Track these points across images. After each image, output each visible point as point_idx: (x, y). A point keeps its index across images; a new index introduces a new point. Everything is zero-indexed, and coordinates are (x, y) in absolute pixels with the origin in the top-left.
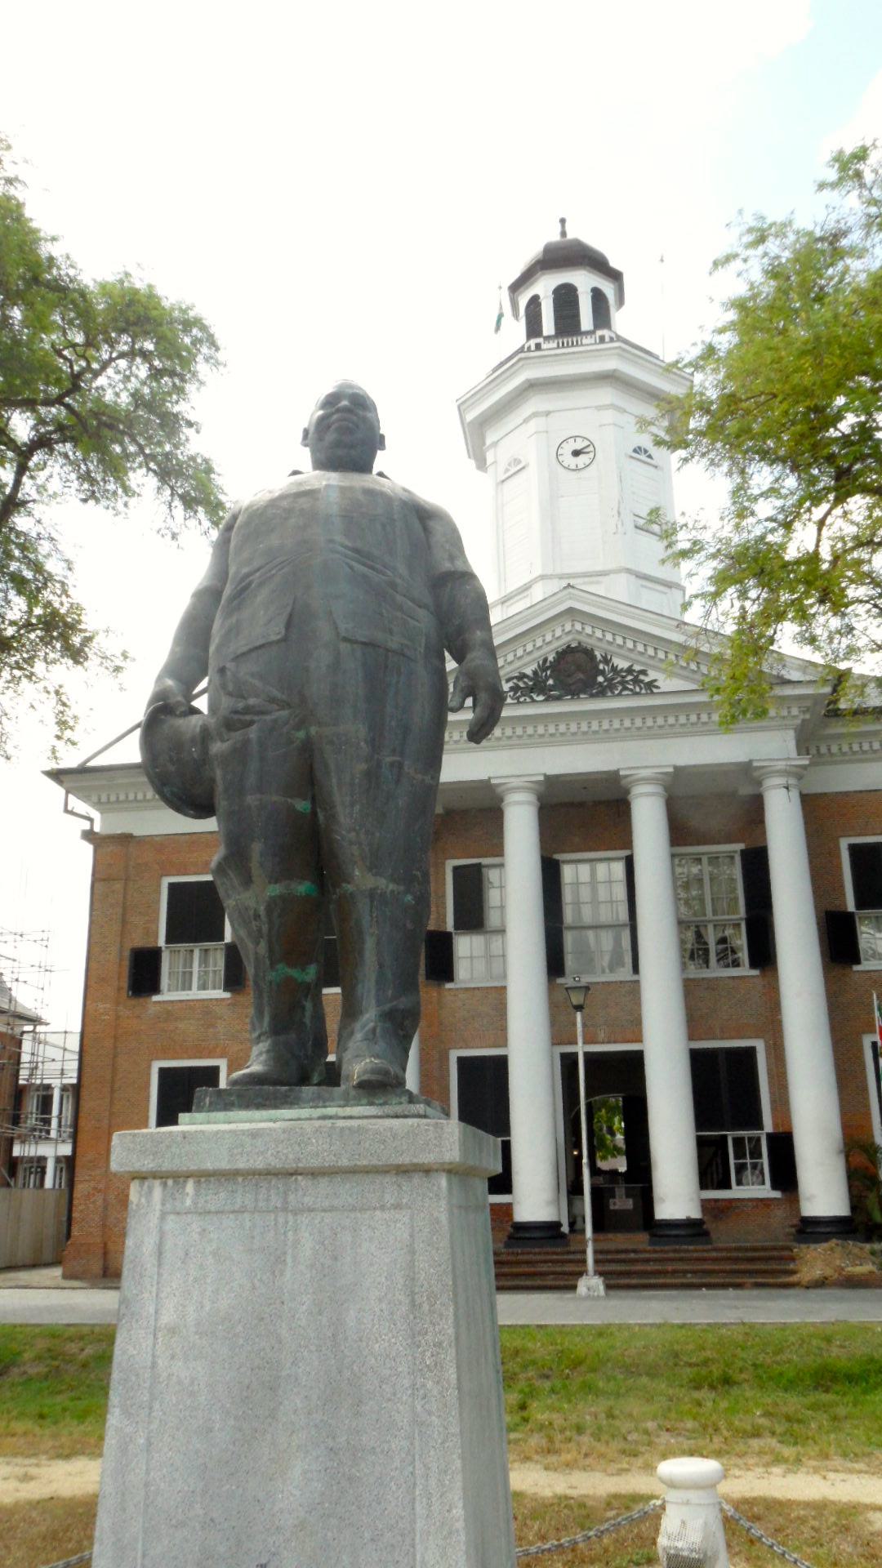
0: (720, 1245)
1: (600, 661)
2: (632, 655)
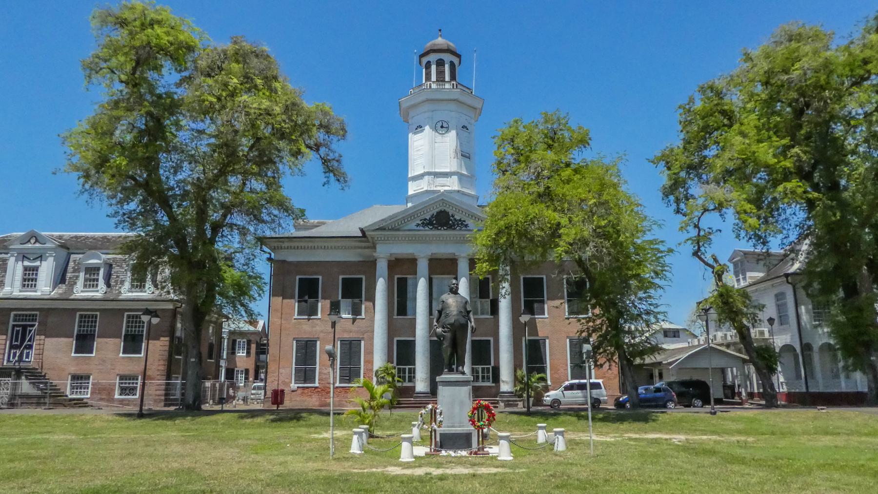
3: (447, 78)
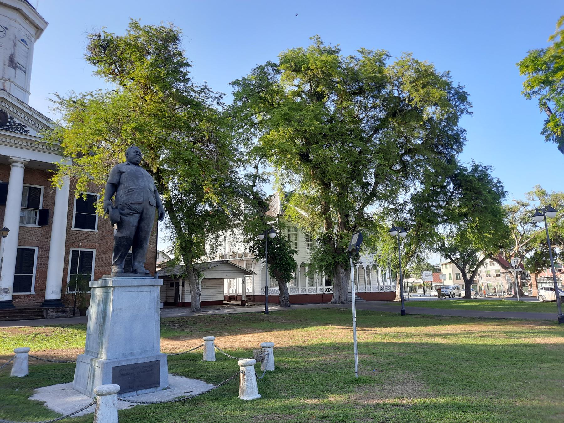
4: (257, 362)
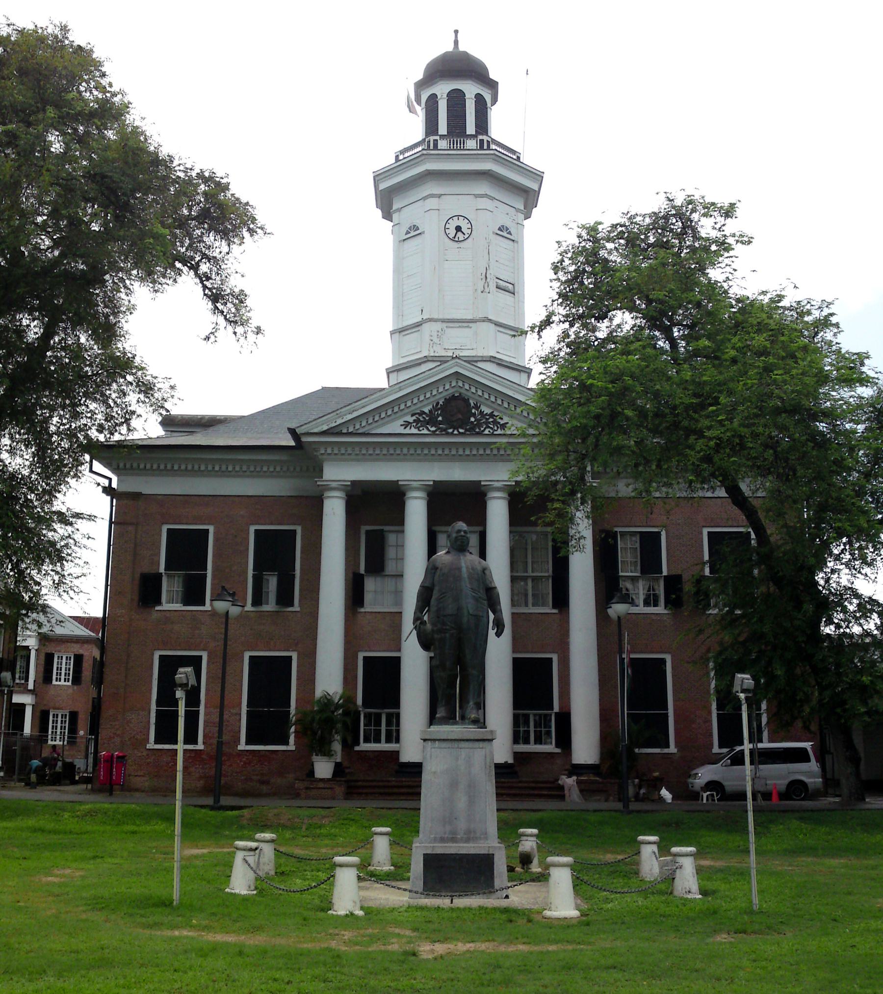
0: (524, 779)
1: (473, 407)
2: (493, 405)
3: (471, 129)
4: (582, 915)
